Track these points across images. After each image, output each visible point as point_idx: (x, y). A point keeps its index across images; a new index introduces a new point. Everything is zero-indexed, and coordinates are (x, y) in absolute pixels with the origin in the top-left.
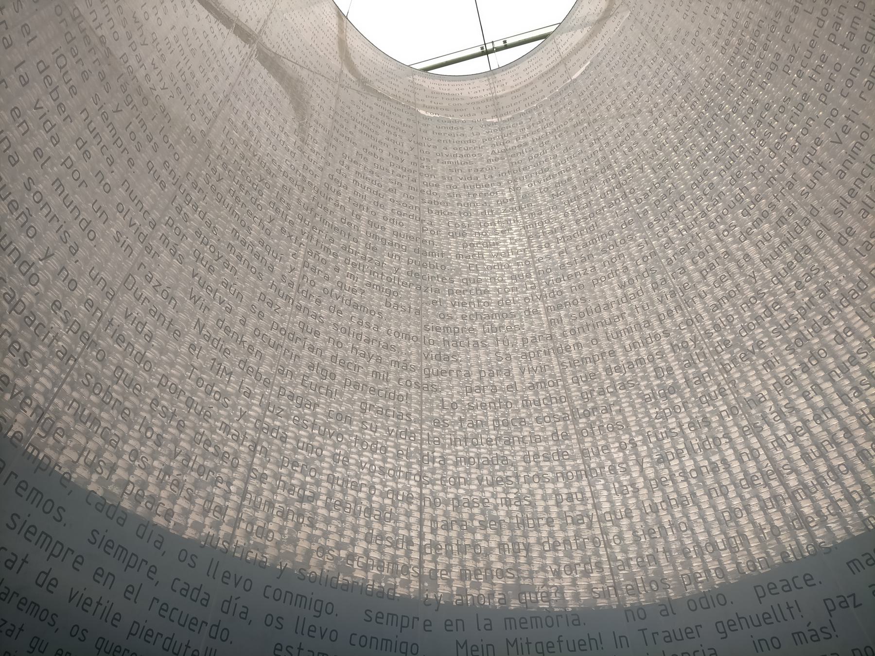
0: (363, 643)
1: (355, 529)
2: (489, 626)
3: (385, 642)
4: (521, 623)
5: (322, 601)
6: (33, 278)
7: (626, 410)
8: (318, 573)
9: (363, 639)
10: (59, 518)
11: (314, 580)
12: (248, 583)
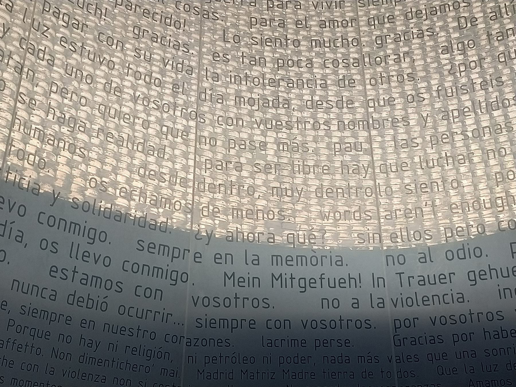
0: (135, 270)
1: (117, 157)
2: (257, 261)
3: (156, 269)
4: (287, 261)
5: (305, 279)
6: (297, 44)
7: (416, 52)
8: (79, 197)
9: (136, 266)
10: (64, 271)
11: (75, 206)
12: (22, 208)
